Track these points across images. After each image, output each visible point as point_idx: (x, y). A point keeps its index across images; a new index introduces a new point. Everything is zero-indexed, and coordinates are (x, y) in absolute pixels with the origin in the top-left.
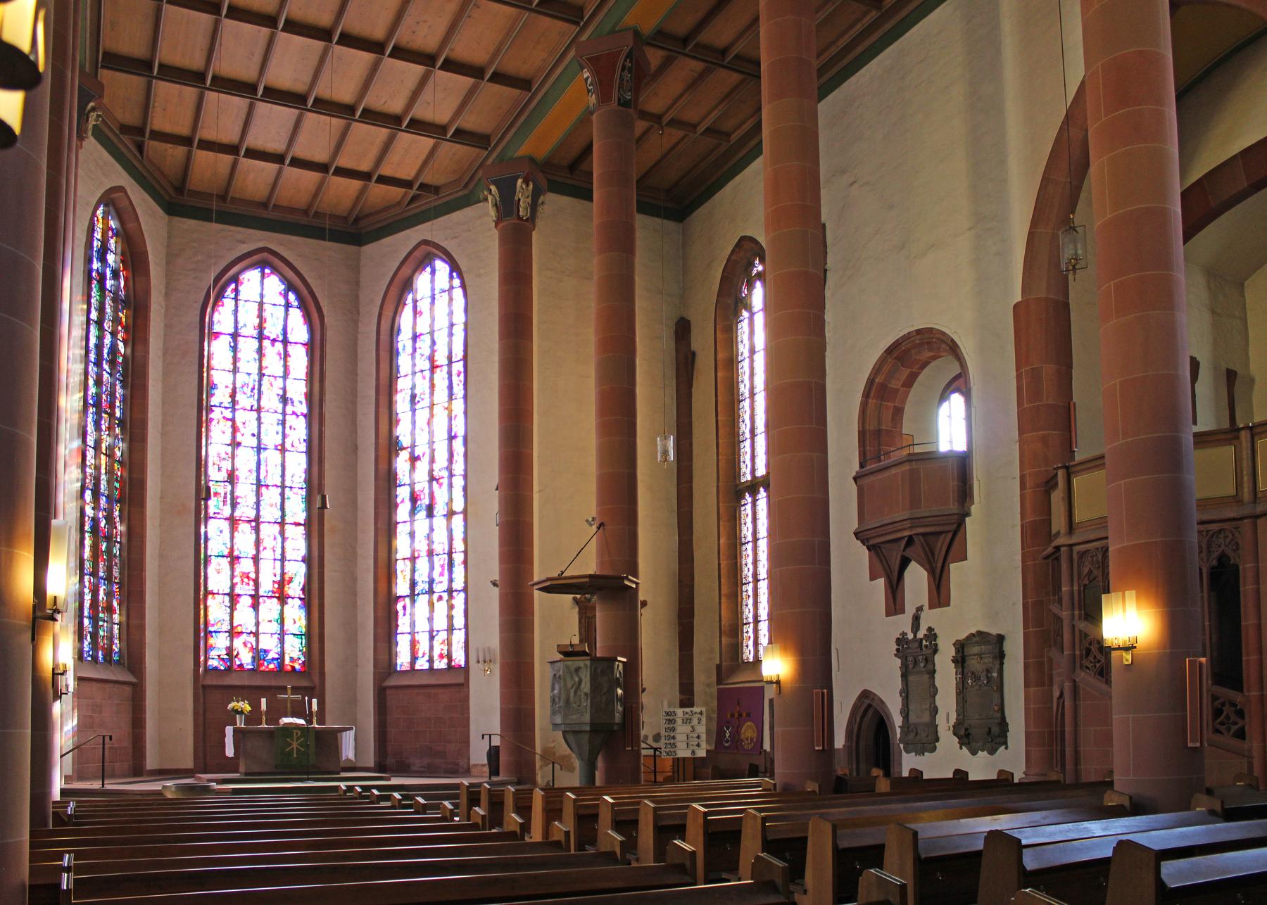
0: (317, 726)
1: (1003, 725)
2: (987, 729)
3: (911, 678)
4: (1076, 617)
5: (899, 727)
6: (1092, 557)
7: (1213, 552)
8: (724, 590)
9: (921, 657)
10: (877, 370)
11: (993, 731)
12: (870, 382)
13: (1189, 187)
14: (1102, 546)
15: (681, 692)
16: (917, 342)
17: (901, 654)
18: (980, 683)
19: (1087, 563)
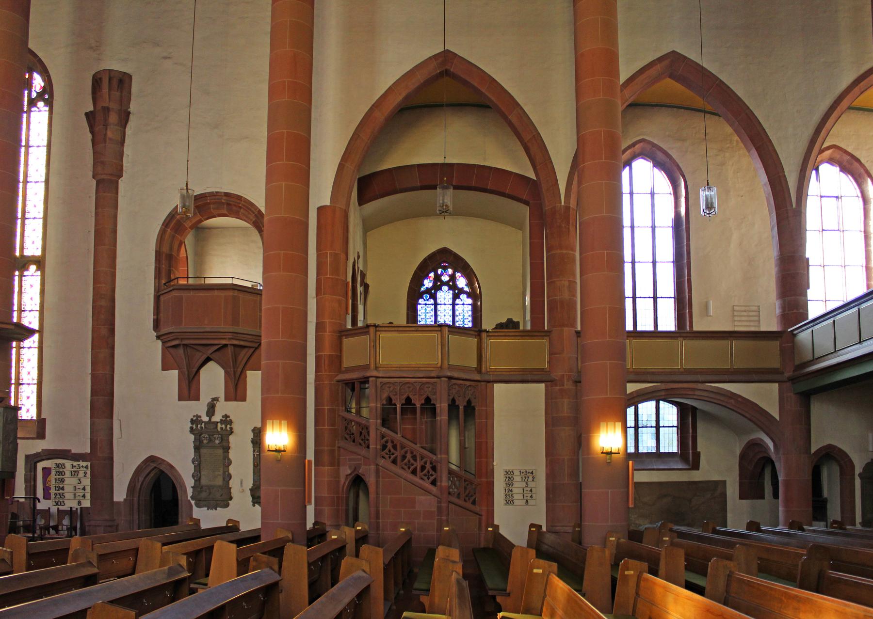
3: (203, 451)
9: (216, 436)
13: (382, 171)
16: (223, 201)
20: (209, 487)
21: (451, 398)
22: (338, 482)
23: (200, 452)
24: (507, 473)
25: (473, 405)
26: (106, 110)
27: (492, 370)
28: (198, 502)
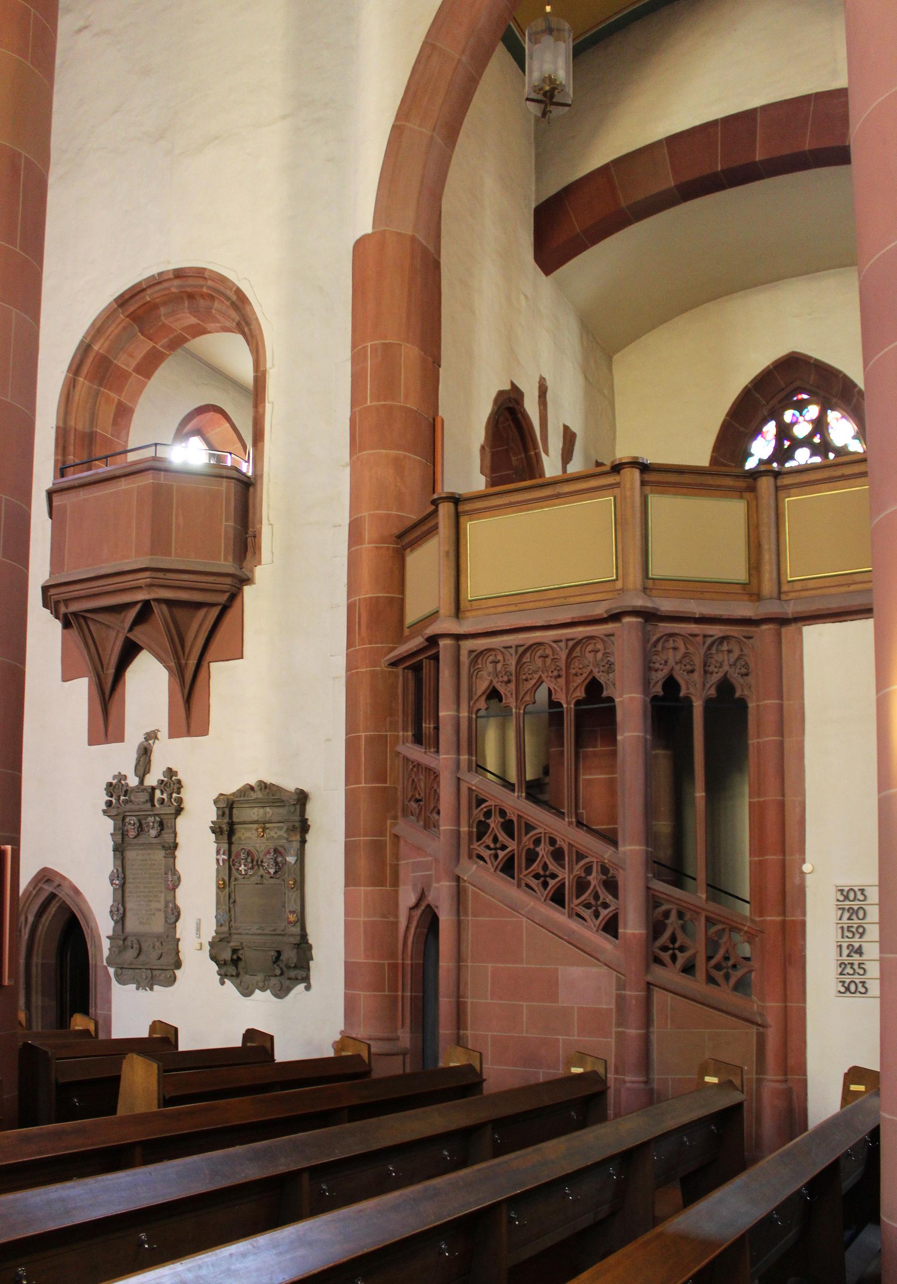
0: (559, 1037)
1: (303, 948)
2: (273, 953)
3: (130, 855)
4: (464, 765)
5: (108, 937)
6: (496, 662)
7: (712, 673)
9: (151, 819)
10: (98, 329)
11: (283, 957)
12: (84, 349)
14: (517, 643)
16: (174, 290)
17: (114, 812)
18: (261, 872)
19: (484, 673)
20: (140, 938)
21: (659, 676)
22: (396, 924)
24: (847, 898)
25: (738, 694)
27: (798, 586)
28: (120, 971)
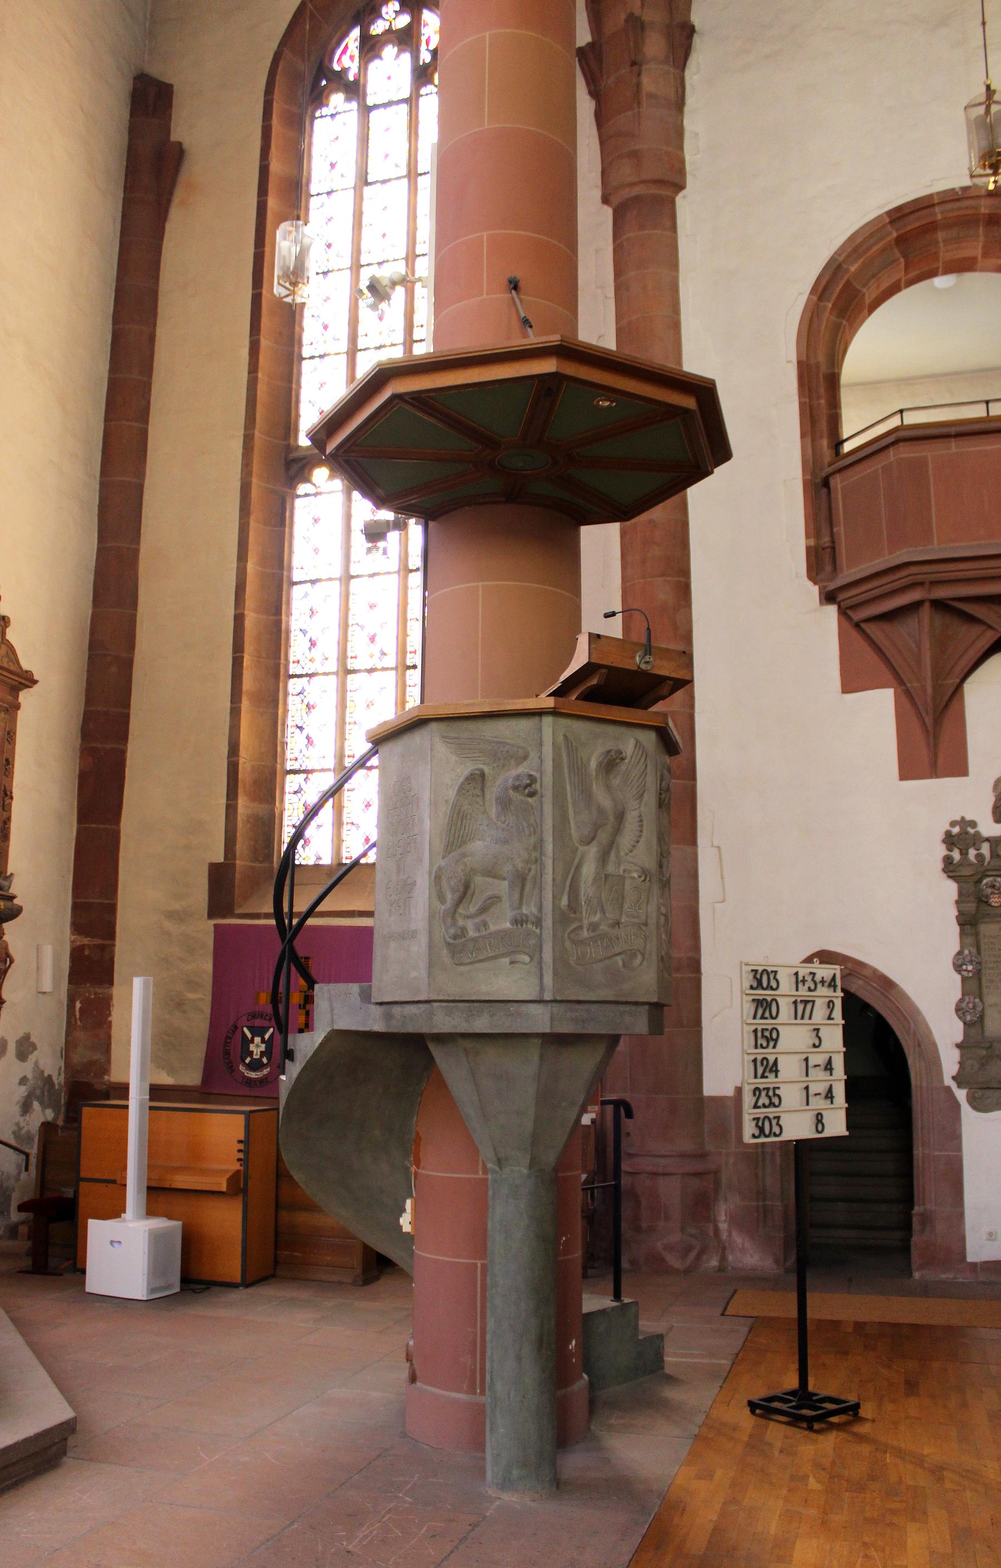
8: (248, 682)
15: (78, 927)
23: (977, 935)
26: (636, 25)
